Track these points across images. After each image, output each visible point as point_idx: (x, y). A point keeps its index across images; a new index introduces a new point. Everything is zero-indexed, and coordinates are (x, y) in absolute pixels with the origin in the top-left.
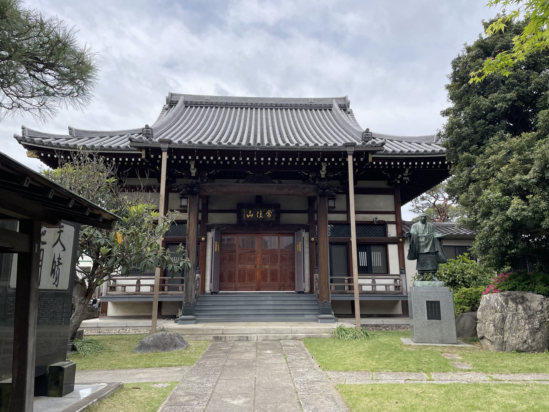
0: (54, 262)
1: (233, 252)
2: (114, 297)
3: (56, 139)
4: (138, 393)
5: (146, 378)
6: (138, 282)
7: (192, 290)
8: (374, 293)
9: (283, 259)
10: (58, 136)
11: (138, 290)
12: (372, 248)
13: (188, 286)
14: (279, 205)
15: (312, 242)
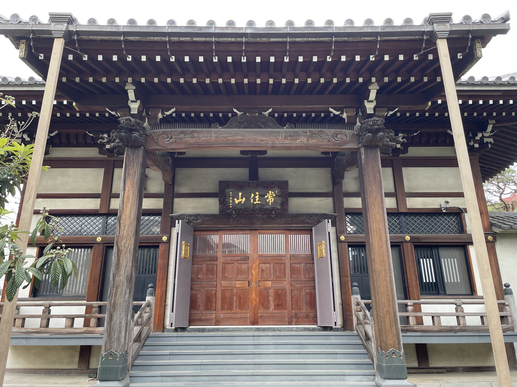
1: (213, 260)
6: (47, 310)
7: (120, 327)
8: (461, 329)
9: (293, 271)
12: (443, 252)
13: (115, 318)
14: (286, 183)
15: (342, 242)
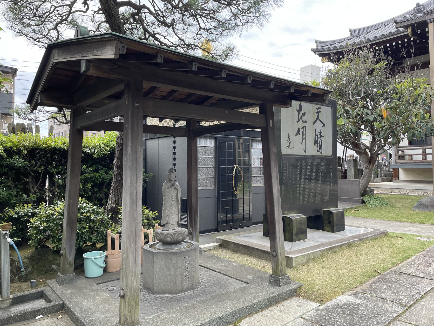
0: (316, 135)
2: (402, 165)
3: (340, 43)
4: (399, 241)
5: (414, 231)
6: (424, 151)
10: (342, 39)
11: (424, 158)
